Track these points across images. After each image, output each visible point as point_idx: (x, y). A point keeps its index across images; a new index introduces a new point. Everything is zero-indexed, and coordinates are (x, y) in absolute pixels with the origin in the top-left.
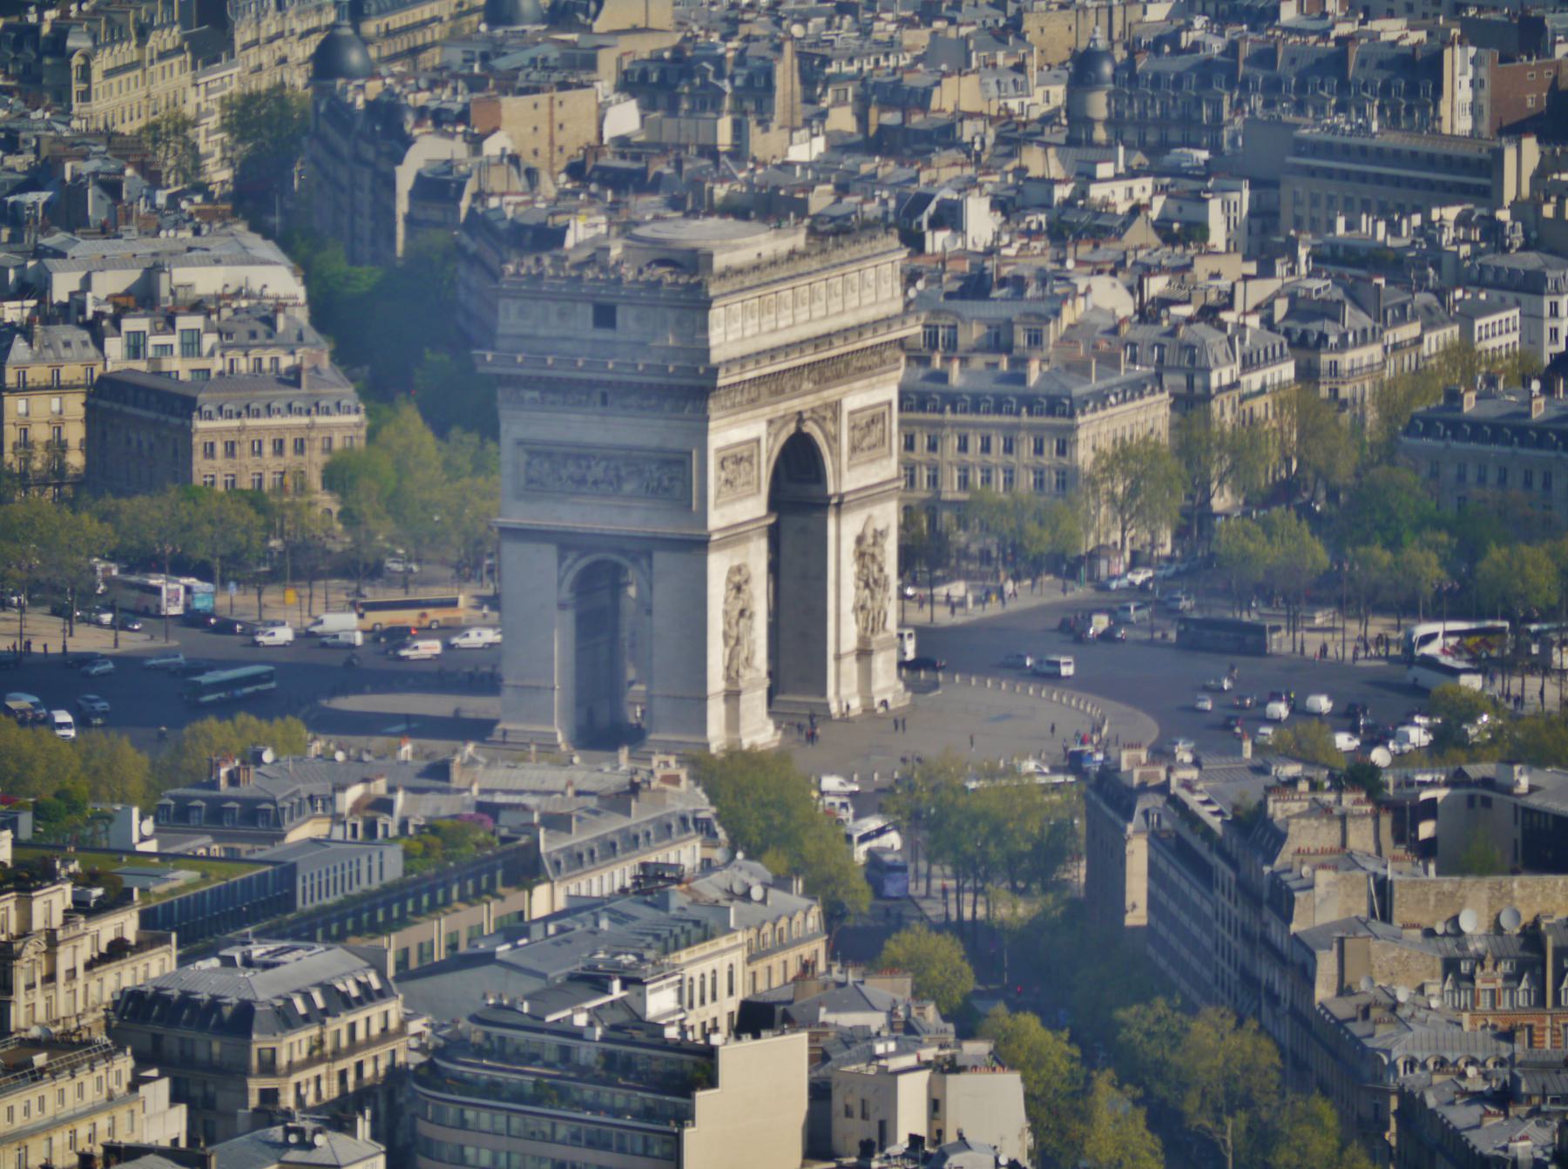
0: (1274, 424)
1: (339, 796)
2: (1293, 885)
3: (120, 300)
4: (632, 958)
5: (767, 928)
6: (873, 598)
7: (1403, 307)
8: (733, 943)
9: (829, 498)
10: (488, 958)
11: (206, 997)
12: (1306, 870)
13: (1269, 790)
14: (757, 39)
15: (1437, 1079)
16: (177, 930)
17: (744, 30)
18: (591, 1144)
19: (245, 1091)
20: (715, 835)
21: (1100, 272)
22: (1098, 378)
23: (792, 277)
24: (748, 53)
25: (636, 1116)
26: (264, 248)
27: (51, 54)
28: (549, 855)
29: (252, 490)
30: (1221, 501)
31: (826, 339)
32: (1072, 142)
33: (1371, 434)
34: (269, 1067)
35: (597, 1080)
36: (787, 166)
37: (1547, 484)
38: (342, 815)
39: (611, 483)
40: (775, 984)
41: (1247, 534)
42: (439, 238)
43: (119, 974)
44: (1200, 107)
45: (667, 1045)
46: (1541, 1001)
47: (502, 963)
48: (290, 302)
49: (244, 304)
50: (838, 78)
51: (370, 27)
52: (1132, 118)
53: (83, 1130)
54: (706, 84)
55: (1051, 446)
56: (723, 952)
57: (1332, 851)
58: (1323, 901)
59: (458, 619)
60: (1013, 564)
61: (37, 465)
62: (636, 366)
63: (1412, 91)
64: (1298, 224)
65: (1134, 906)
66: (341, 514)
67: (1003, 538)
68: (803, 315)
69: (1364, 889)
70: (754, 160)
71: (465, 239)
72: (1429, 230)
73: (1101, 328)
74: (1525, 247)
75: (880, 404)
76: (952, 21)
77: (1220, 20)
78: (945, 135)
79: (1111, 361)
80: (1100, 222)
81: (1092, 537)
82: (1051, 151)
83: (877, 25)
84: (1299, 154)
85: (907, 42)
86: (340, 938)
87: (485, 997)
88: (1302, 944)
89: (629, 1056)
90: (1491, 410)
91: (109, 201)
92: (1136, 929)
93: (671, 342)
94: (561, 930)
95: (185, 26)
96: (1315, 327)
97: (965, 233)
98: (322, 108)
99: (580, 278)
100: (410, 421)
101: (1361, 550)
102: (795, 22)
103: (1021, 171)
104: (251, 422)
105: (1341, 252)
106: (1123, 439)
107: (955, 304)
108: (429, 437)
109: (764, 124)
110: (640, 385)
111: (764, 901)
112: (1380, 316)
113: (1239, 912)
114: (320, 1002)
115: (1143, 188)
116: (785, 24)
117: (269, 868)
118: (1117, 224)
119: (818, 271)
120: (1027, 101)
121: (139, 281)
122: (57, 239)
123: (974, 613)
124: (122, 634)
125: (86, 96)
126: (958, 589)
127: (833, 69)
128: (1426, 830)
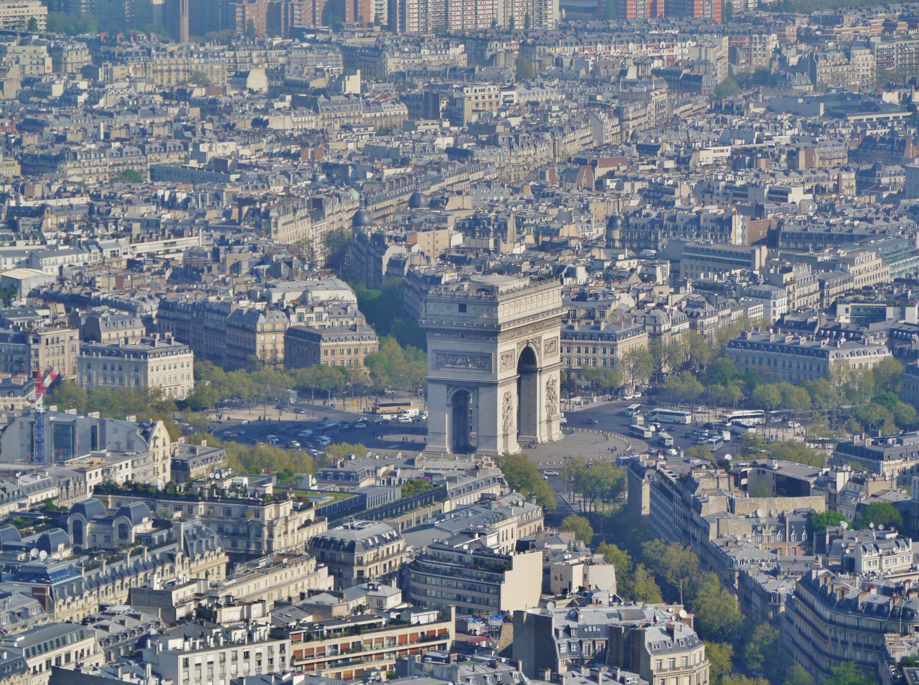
12: (705, 496)
15: (752, 566)
18: (469, 589)
19: (352, 571)
25: (485, 580)
32: (607, 247)
34: (360, 563)
35: (472, 568)
36: (513, 255)
37: (775, 364)
40: (522, 536)
42: (398, 280)
45: (495, 556)
46: (785, 540)
47: (437, 528)
50: (528, 225)
51: (370, 208)
53: (300, 585)
54: (484, 228)
55: (608, 351)
61: (268, 357)
63: (722, 230)
64: (686, 275)
71: (407, 281)
72: (732, 278)
74: (764, 283)
76: (565, 206)
77: (655, 206)
78: (564, 245)
79: (628, 322)
83: (540, 207)
86: (381, 519)
89: (482, 560)
90: (757, 339)
92: (644, 516)
93: (485, 316)
94: (455, 516)
96: (696, 310)
98: (356, 236)
100: (393, 343)
103: (592, 257)
107: (575, 303)
108: (399, 348)
112: (717, 307)
113: (682, 510)
114: (377, 542)
115: (634, 263)
122: (272, 281)
123: (584, 407)
125: (276, 232)
127: (526, 222)
128: (744, 481)
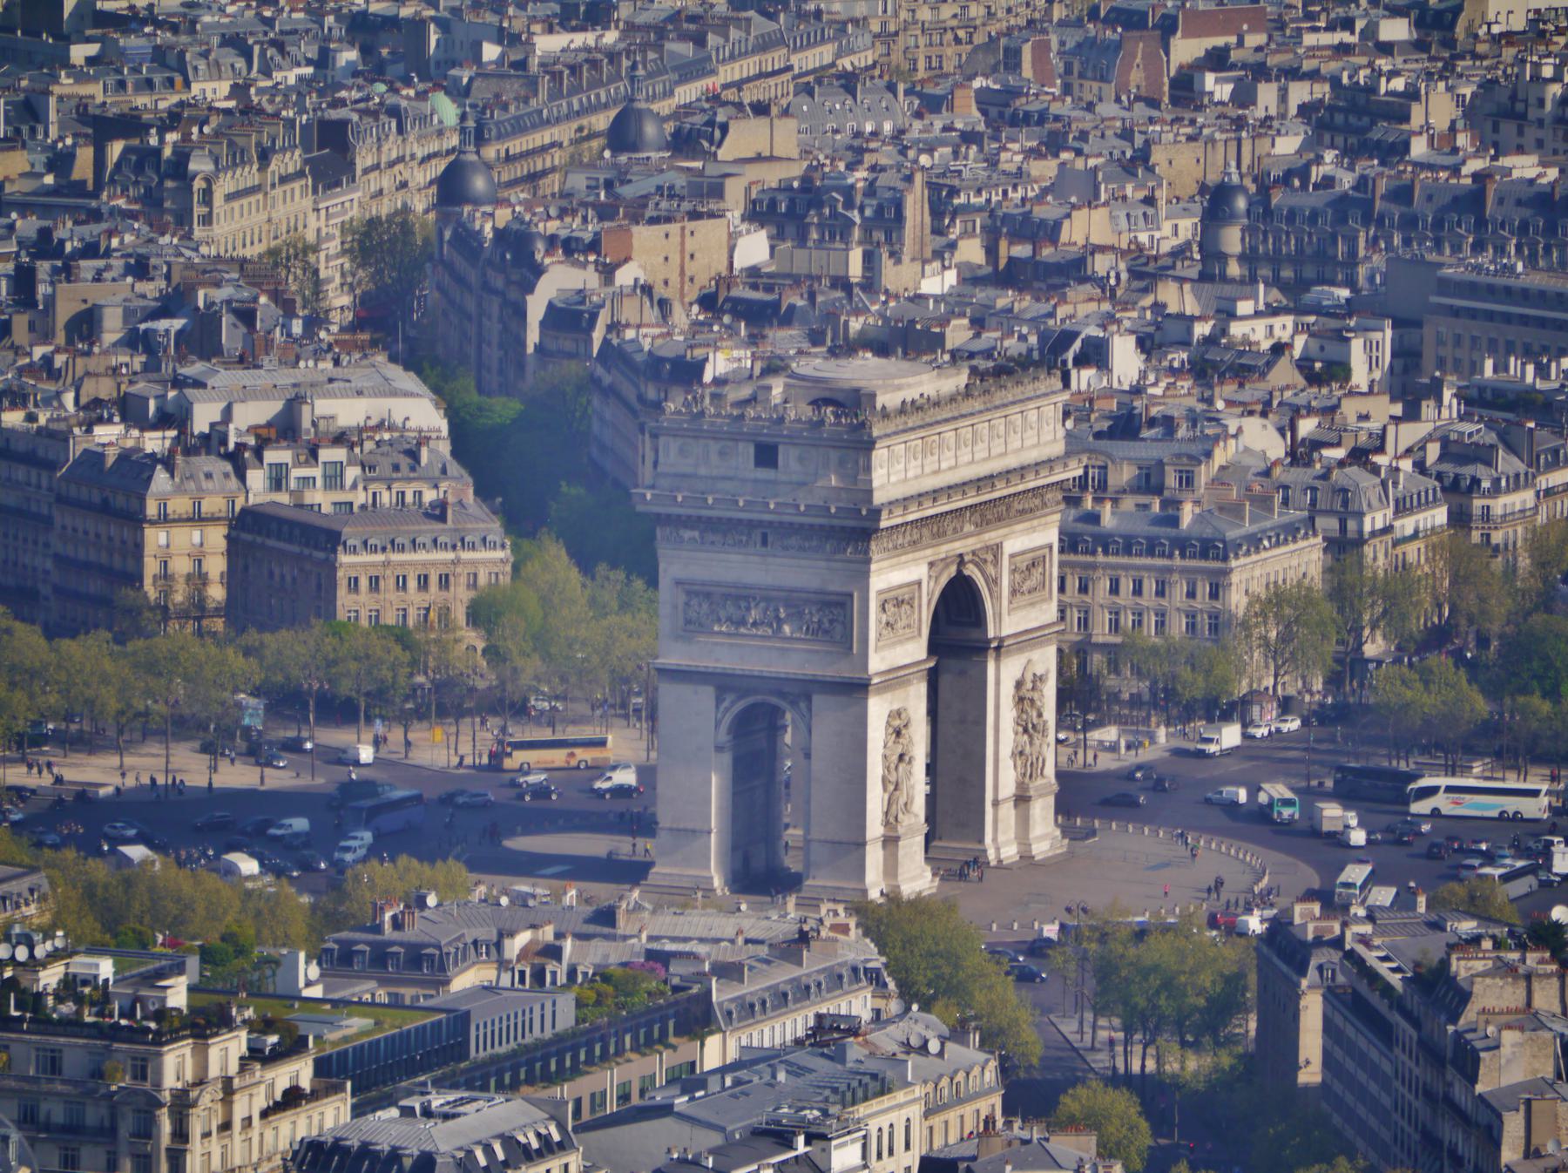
0: (1427, 569)
1: (507, 942)
2: (1478, 1045)
3: (260, 431)
4: (816, 1113)
5: (945, 1082)
6: (1031, 743)
7: (1556, 452)
8: (910, 1097)
9: (989, 641)
10: (666, 1110)
11: (387, 1148)
12: (1491, 1030)
13: (1451, 947)
14: (883, 169)
16: (352, 1078)
17: (869, 159)
20: (885, 985)
21: (1251, 413)
22: (1252, 522)
23: (955, 418)
24: (878, 183)
26: (406, 379)
27: (173, 177)
28: (720, 1004)
29: (397, 626)
31: (989, 480)
32: (1205, 277)
33: (1523, 580)
36: (919, 298)
38: (510, 961)
39: (771, 626)
41: (1403, 682)
43: (294, 1123)
44: (1335, 243)
47: (681, 1116)
48: (434, 435)
49: (387, 436)
50: (967, 209)
52: (1288, 255)
54: (834, 214)
55: (1203, 589)
56: (900, 1106)
57: (1517, 1011)
58: (1508, 1061)
59: (607, 759)
60: (1165, 709)
61: (179, 598)
62: (797, 507)
65: (1308, 1063)
66: (484, 651)
67: (1154, 683)
68: (965, 457)
69: (1551, 1050)
70: (887, 292)
73: (1253, 470)
75: (1041, 548)
76: (1079, 152)
77: (1350, 154)
78: (1075, 269)
79: (1264, 502)
80: (1243, 361)
81: (1245, 683)
82: (1187, 287)
83: (1004, 156)
84: (1441, 294)
85: (1034, 173)
86: (514, 1086)
87: (669, 1151)
88: (1488, 1105)
91: (243, 329)
92: (1307, 1088)
93: (834, 481)
94: (737, 1082)
95: (307, 150)
96: (1468, 471)
97: (1110, 371)
98: (447, 235)
99: (742, 417)
100: (555, 560)
101: (1521, 699)
102: (921, 151)
103: (1158, 307)
104: (396, 557)
105: (1488, 395)
106: (1276, 582)
108: (574, 574)
109: (896, 256)
110: (802, 525)
111: (941, 1054)
112: (1533, 462)
115: (1283, 326)
116: (911, 154)
117: (443, 1016)
118: (1261, 363)
119: (981, 412)
120: (1157, 235)
121: (277, 416)
122: (195, 369)
123: (1128, 759)
124: (268, 771)
125: (207, 220)
126: (1110, 734)
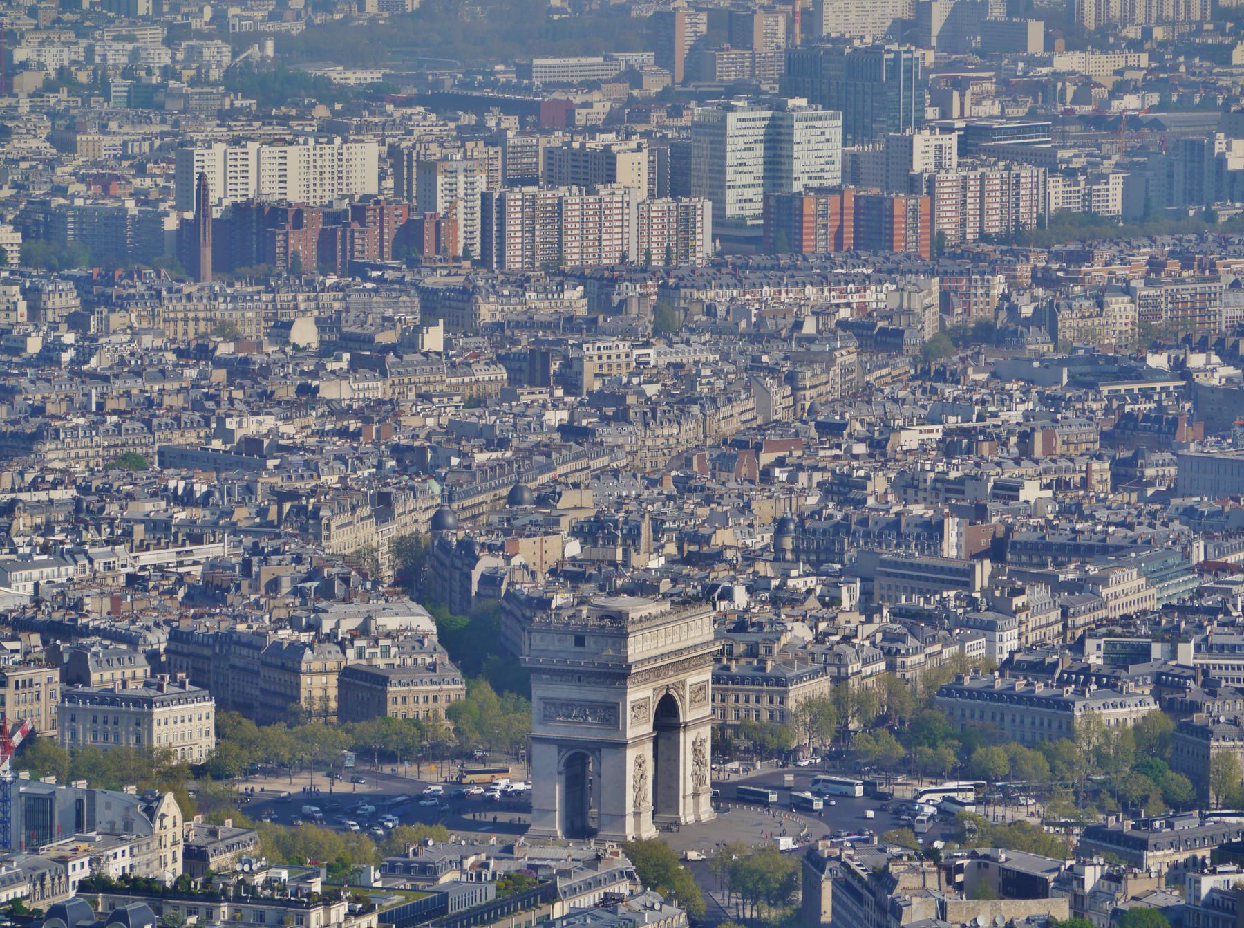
27: (312, 518)
30: (853, 725)
32: (776, 560)
36: (648, 570)
37: (1002, 719)
50: (669, 529)
51: (455, 506)
54: (610, 532)
55: (777, 699)
61: (316, 707)
63: (930, 537)
64: (882, 598)
68: (669, 641)
71: (505, 604)
72: (943, 601)
76: (719, 504)
77: (840, 505)
78: (718, 556)
79: (803, 660)
90: (977, 685)
92: (825, 924)
94: (569, 924)
96: (894, 646)
100: (485, 689)
103: (755, 573)
107: (732, 635)
108: (494, 695)
111: (660, 910)
112: (924, 641)
115: (811, 581)
122: (323, 604)
125: (328, 538)
126: (735, 765)
128: (959, 878)
